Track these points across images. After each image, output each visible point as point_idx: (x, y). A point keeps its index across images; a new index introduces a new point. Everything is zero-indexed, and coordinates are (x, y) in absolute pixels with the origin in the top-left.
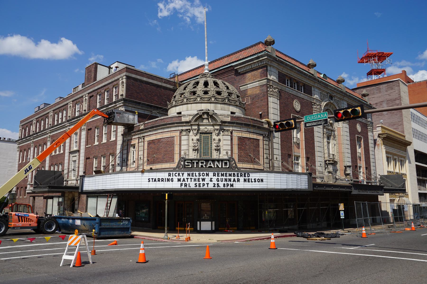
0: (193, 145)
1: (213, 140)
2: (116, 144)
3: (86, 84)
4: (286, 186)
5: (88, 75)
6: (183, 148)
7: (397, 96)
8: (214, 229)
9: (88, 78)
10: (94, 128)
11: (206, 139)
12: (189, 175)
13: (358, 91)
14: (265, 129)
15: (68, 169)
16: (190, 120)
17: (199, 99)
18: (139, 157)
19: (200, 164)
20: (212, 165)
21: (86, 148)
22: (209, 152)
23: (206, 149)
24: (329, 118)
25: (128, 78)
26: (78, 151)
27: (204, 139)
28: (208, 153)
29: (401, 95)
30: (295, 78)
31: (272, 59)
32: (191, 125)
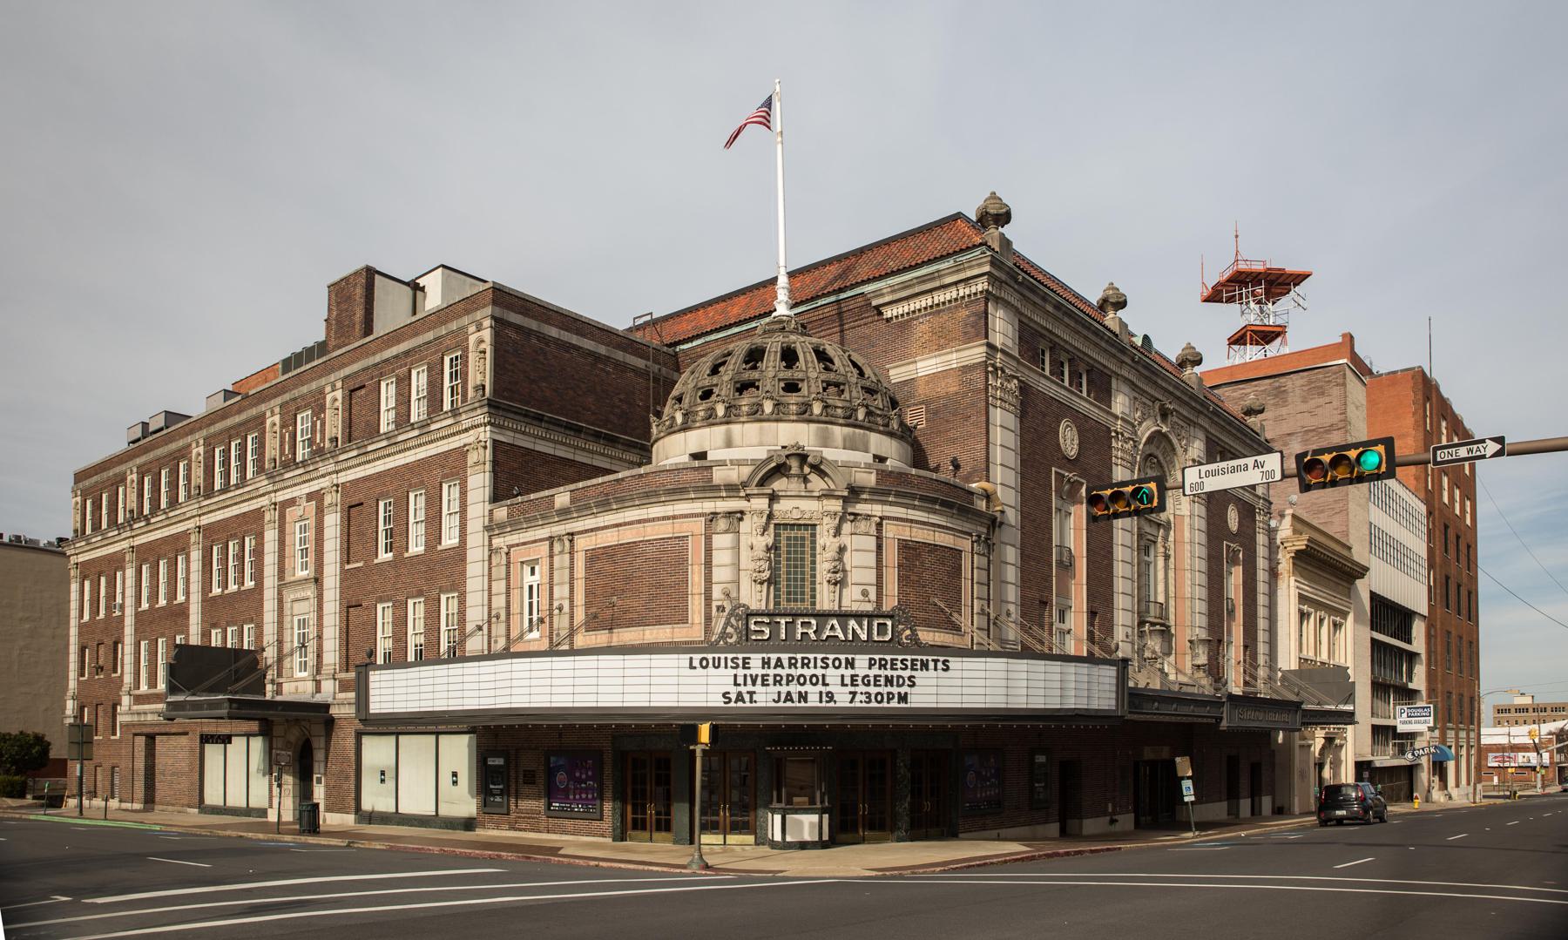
0: (752, 566)
1: (818, 550)
2: (464, 559)
3: (332, 343)
4: (1024, 700)
5: (340, 312)
7: (1336, 418)
8: (826, 837)
9: (339, 322)
12: (766, 663)
14: (979, 514)
15: (280, 642)
18: (556, 604)
21: (346, 576)
22: (807, 590)
25: (499, 324)
26: (318, 581)
27: (788, 546)
28: (803, 593)
31: (1003, 277)
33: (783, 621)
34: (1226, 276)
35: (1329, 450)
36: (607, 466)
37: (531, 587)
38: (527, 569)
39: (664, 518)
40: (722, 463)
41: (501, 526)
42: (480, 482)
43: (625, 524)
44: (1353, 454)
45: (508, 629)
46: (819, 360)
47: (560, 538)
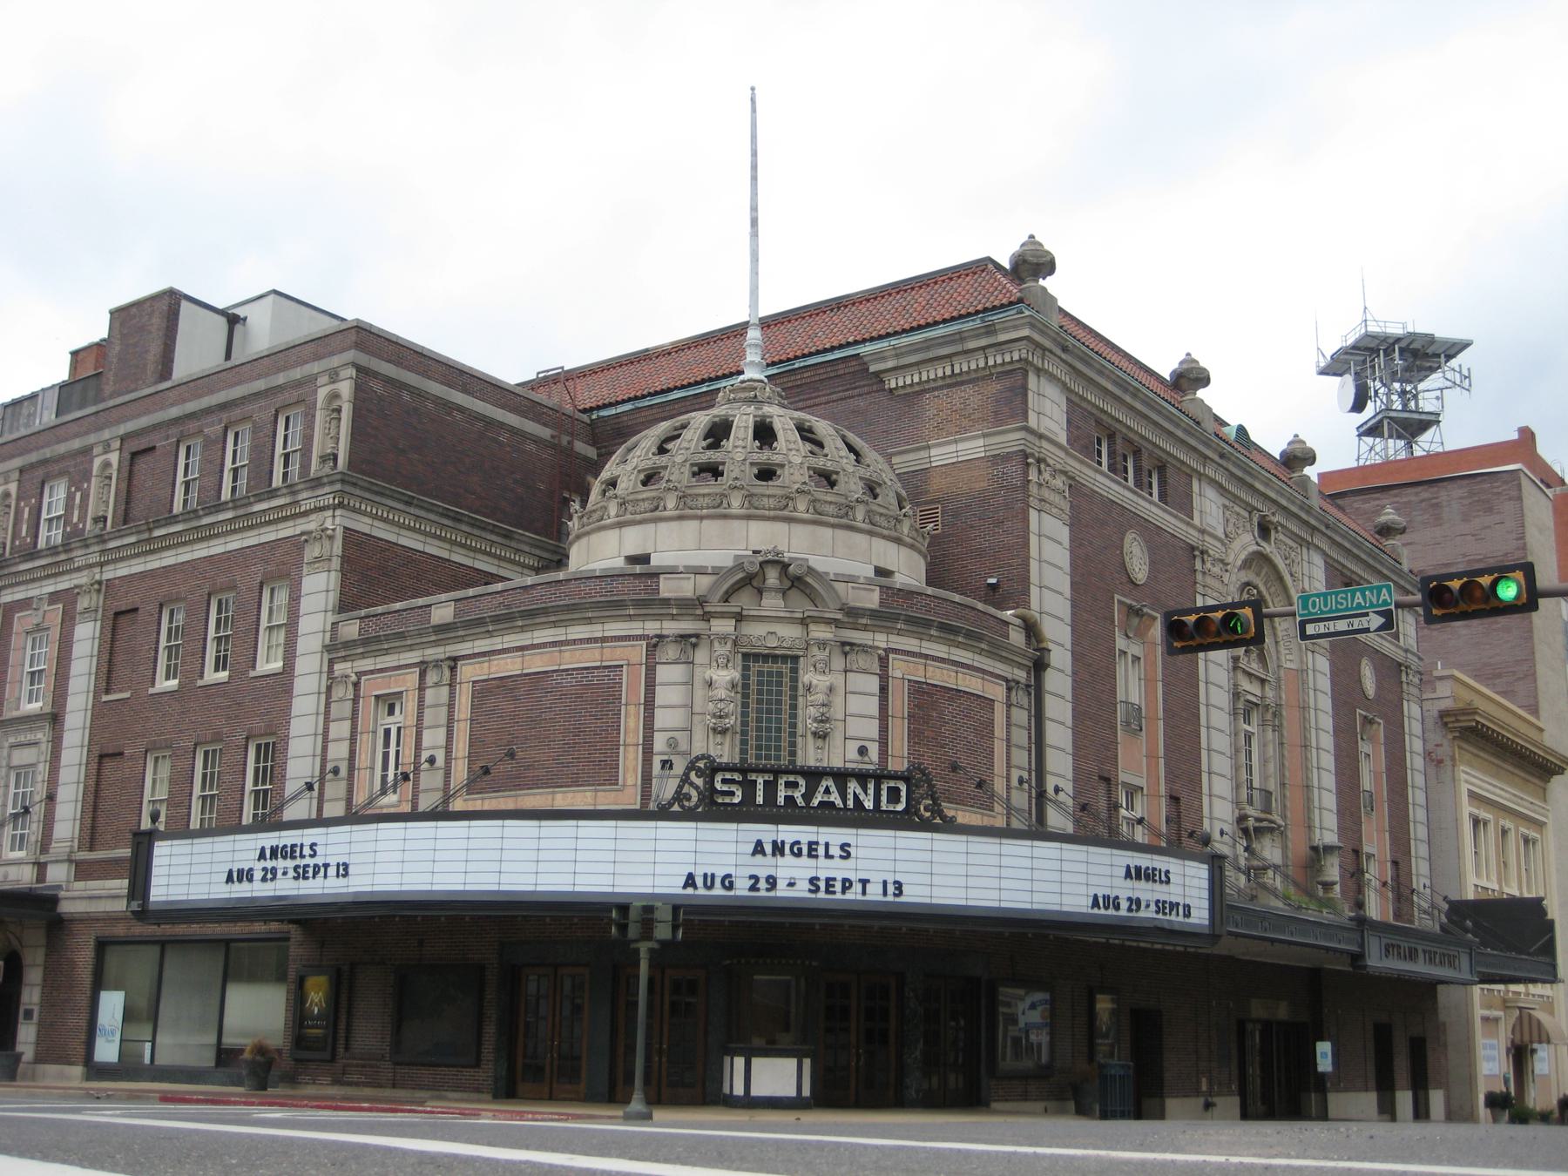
1: (801, 691)
2: (288, 691)
6: (662, 718)
8: (806, 1092)
10: (154, 608)
11: (769, 683)
13: (1356, 503)
17: (736, 501)
18: (425, 755)
20: (835, 798)
21: (99, 712)
22: (784, 744)
24: (1398, 606)
26: (55, 719)
27: (760, 683)
29: (1528, 538)
30: (1131, 435)
32: (707, 617)
33: (760, 780)
34: (1350, 341)
35: (1459, 576)
36: (493, 570)
37: (387, 732)
38: (384, 709)
40: (672, 571)
41: (348, 645)
42: (319, 588)
43: (533, 646)
44: (1485, 581)
45: (350, 791)
46: (803, 438)
47: (437, 664)
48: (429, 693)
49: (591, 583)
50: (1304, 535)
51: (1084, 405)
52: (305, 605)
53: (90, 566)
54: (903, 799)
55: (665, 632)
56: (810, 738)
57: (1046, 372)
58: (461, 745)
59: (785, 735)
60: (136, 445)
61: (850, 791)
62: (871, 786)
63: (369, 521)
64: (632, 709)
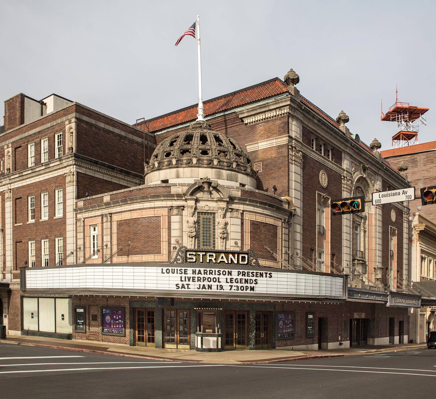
0: (188, 230)
1: (216, 224)
2: (65, 223)
3: (7, 127)
9: (9, 118)
11: (206, 222)
12: (194, 272)
14: (285, 210)
16: (185, 192)
18: (105, 244)
19: (208, 258)
20: (225, 260)
21: (15, 229)
22: (212, 241)
23: (207, 236)
25: (79, 121)
27: (203, 222)
28: (210, 242)
31: (296, 107)
36: (126, 185)
37: (94, 236)
38: (92, 228)
39: (150, 208)
40: (175, 185)
41: (81, 209)
42: (71, 190)
43: (134, 210)
45: (84, 254)
47: (106, 215)
48: (104, 224)
49: (150, 189)
50: (376, 171)
51: (308, 128)
52: (68, 196)
53: (7, 184)
54: (247, 260)
55: (173, 205)
56: (219, 238)
57: (295, 116)
58: (115, 241)
59: (211, 238)
60: (16, 145)
61: (230, 258)
62: (236, 256)
63: (85, 169)
64: (164, 230)
